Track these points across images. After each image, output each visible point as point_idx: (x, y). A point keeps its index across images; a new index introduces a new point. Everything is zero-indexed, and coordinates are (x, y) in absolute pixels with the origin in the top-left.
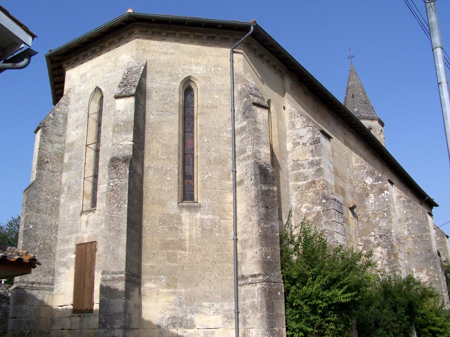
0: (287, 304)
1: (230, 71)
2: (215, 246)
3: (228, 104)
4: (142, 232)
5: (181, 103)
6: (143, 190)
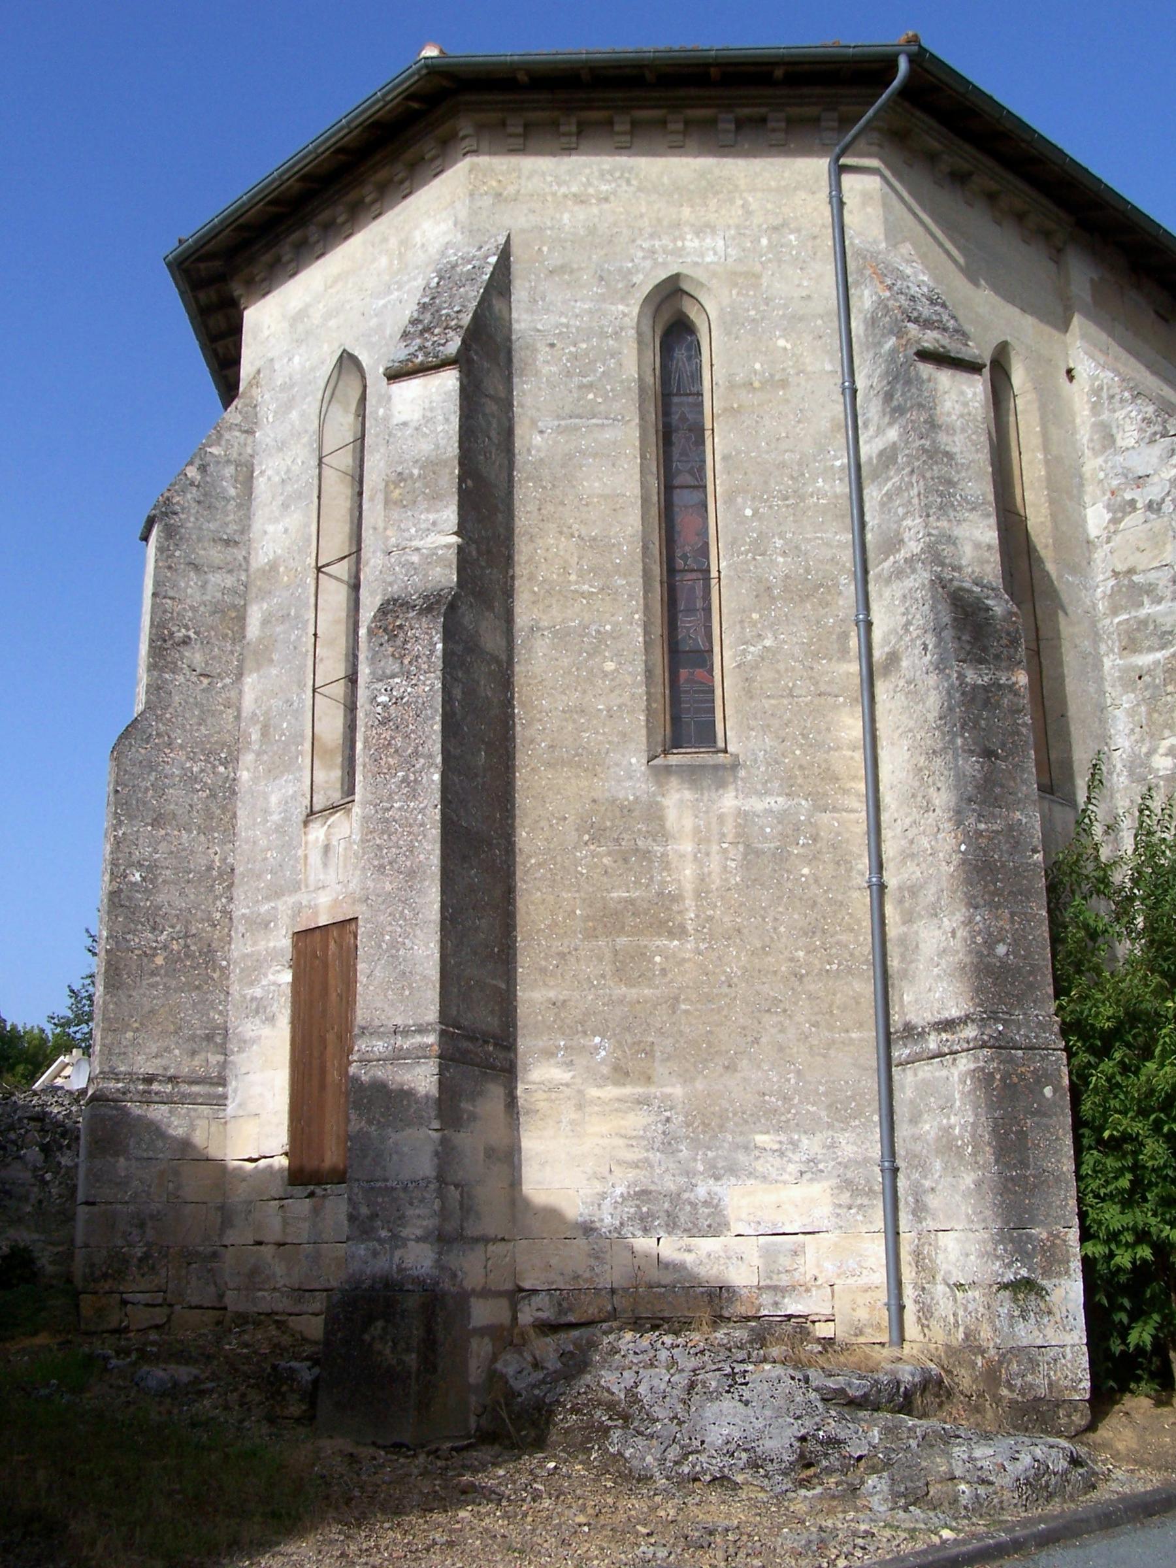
0: (1083, 1136)
1: (830, 243)
2: (796, 916)
3: (828, 367)
4: (514, 874)
5: (650, 380)
6: (512, 716)
